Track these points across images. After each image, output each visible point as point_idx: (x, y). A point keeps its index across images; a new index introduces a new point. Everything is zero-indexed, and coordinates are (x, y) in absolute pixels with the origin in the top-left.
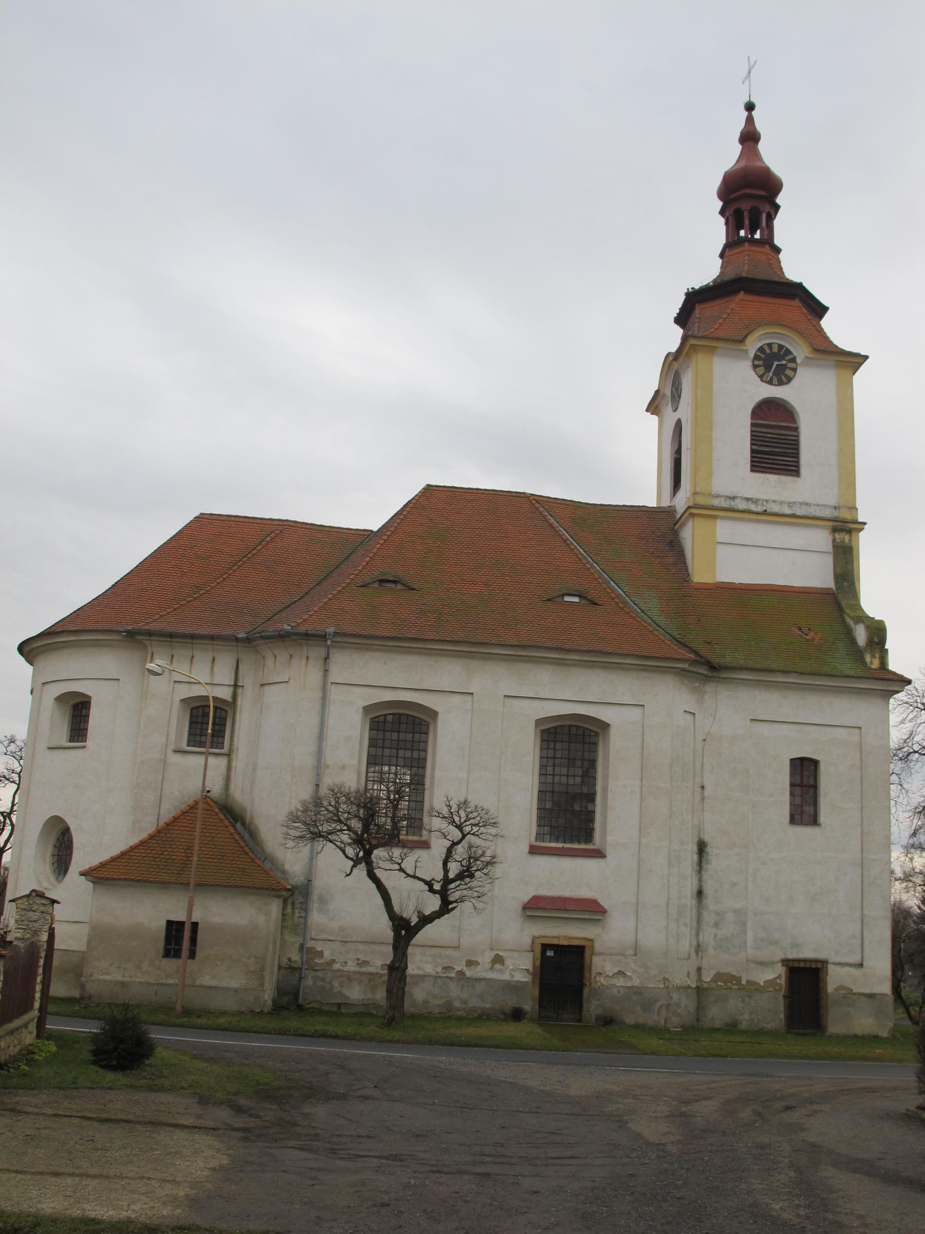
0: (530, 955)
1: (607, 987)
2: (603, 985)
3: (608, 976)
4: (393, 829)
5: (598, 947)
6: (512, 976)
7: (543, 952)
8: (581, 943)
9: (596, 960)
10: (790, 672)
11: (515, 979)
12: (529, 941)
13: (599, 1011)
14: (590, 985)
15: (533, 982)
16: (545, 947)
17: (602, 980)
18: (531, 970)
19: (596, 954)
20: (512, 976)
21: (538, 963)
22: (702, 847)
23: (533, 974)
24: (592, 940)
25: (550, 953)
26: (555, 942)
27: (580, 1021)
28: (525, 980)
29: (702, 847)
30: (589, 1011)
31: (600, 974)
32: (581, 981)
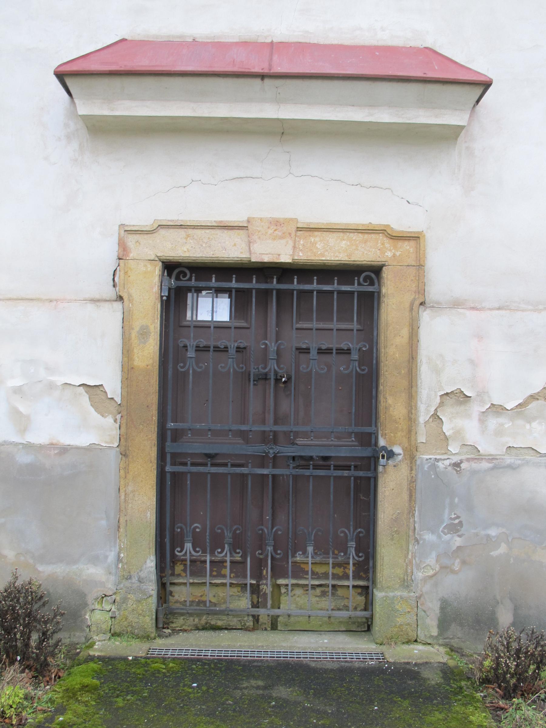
0: (111, 317)
1: (497, 466)
2: (475, 454)
3: (497, 409)
4: (103, 662)
5: (444, 274)
6: (22, 421)
7: (174, 303)
8: (360, 253)
9: (438, 336)
10: (75, 448)
11: (38, 437)
12: (108, 251)
13: (459, 584)
14: (411, 455)
15: (125, 441)
16: (184, 278)
17: (467, 428)
18: (114, 388)
19: (437, 307)
20: (22, 421)
21: (148, 352)
22: (409, 203)
23: (126, 412)
24: (415, 238)
25: (213, 309)
26: (229, 249)
27: (366, 627)
28: (84, 439)
29: (409, 203)
30: (406, 583)
31: (460, 398)
32: (368, 439)
